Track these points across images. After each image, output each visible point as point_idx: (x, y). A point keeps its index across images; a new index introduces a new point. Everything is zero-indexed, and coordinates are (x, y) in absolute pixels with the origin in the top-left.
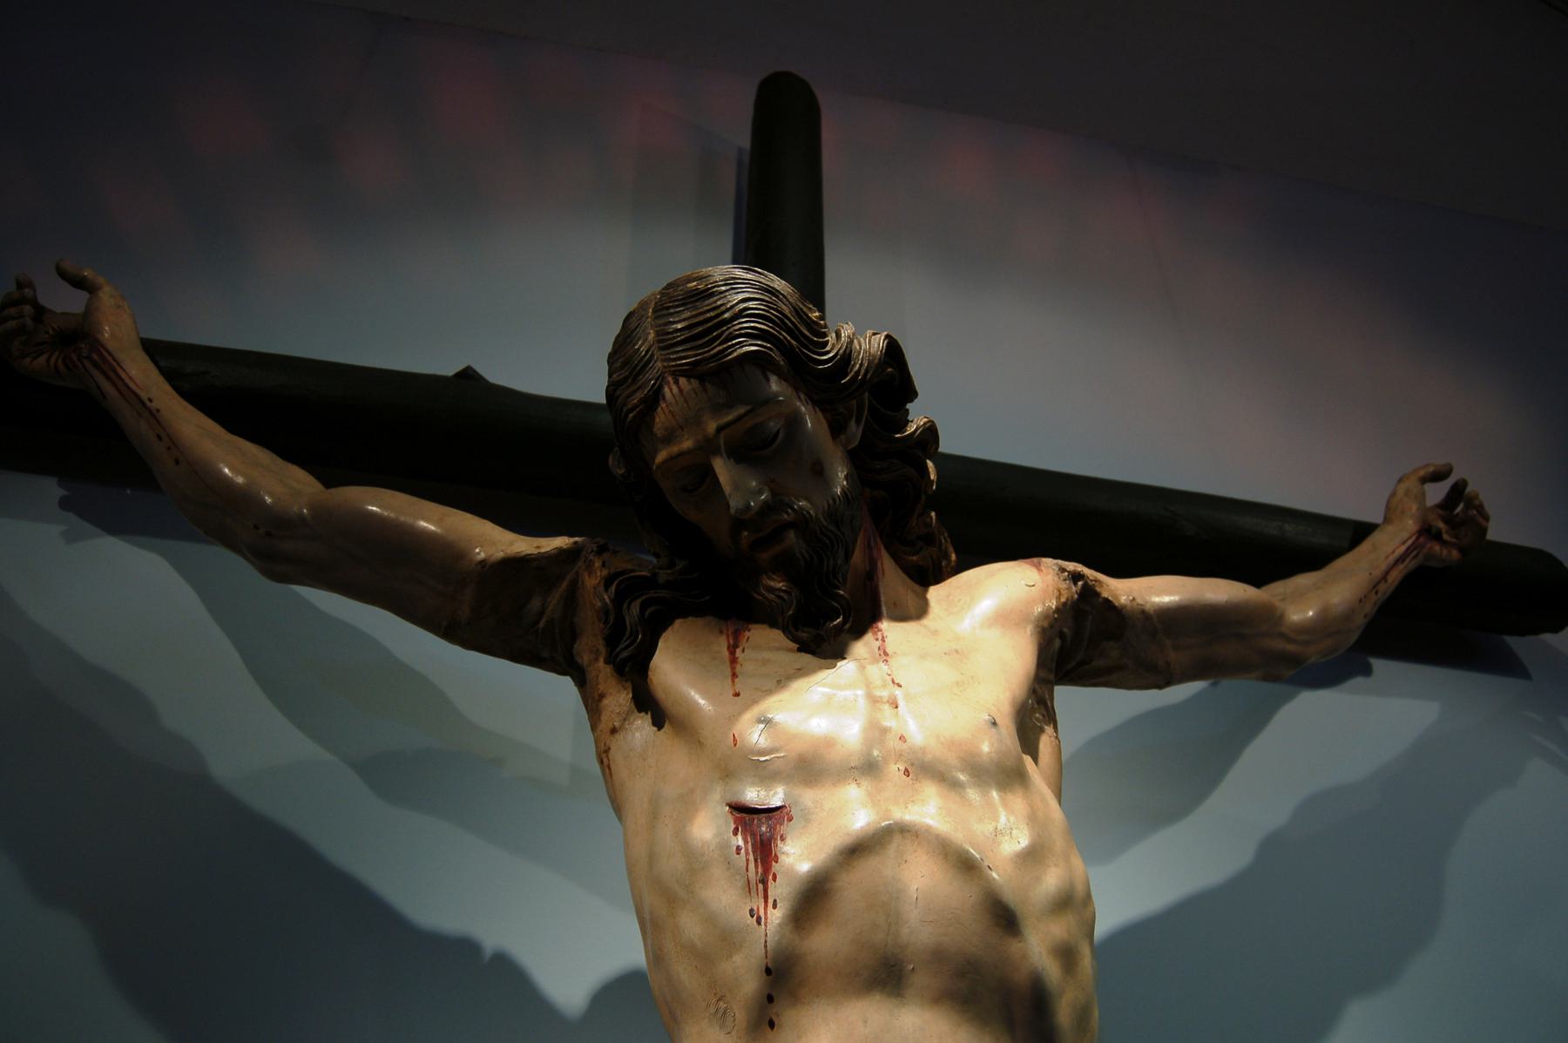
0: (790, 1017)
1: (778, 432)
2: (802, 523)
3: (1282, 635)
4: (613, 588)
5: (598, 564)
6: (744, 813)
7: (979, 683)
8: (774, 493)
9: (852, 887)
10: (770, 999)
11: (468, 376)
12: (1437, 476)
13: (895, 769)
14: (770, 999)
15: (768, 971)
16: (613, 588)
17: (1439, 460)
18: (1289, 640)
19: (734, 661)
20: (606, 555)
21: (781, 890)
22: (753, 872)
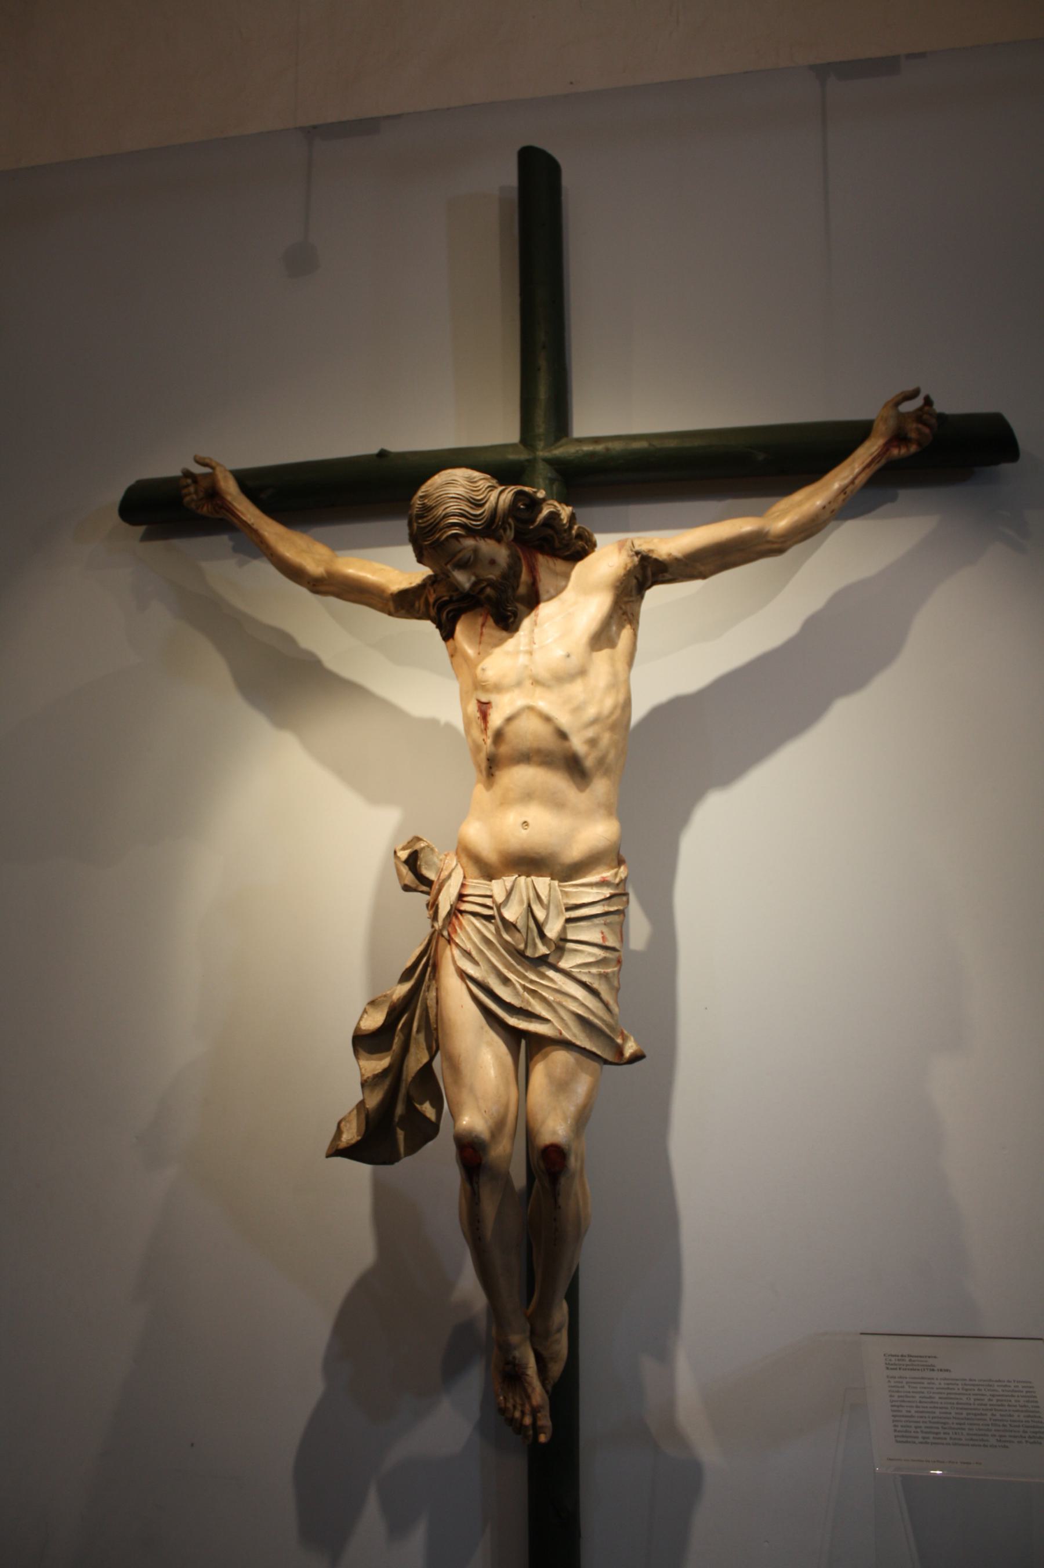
0: (497, 773)
1: (470, 557)
2: (491, 584)
3: (768, 542)
4: (436, 606)
5: (432, 591)
6: (479, 702)
7: (531, 670)
8: (477, 576)
9: (510, 731)
10: (490, 768)
11: (383, 454)
12: (913, 395)
13: (528, 683)
14: (490, 768)
15: (488, 760)
16: (436, 606)
17: (910, 387)
18: (773, 543)
19: (481, 634)
20: (435, 586)
21: (490, 733)
22: (483, 726)
